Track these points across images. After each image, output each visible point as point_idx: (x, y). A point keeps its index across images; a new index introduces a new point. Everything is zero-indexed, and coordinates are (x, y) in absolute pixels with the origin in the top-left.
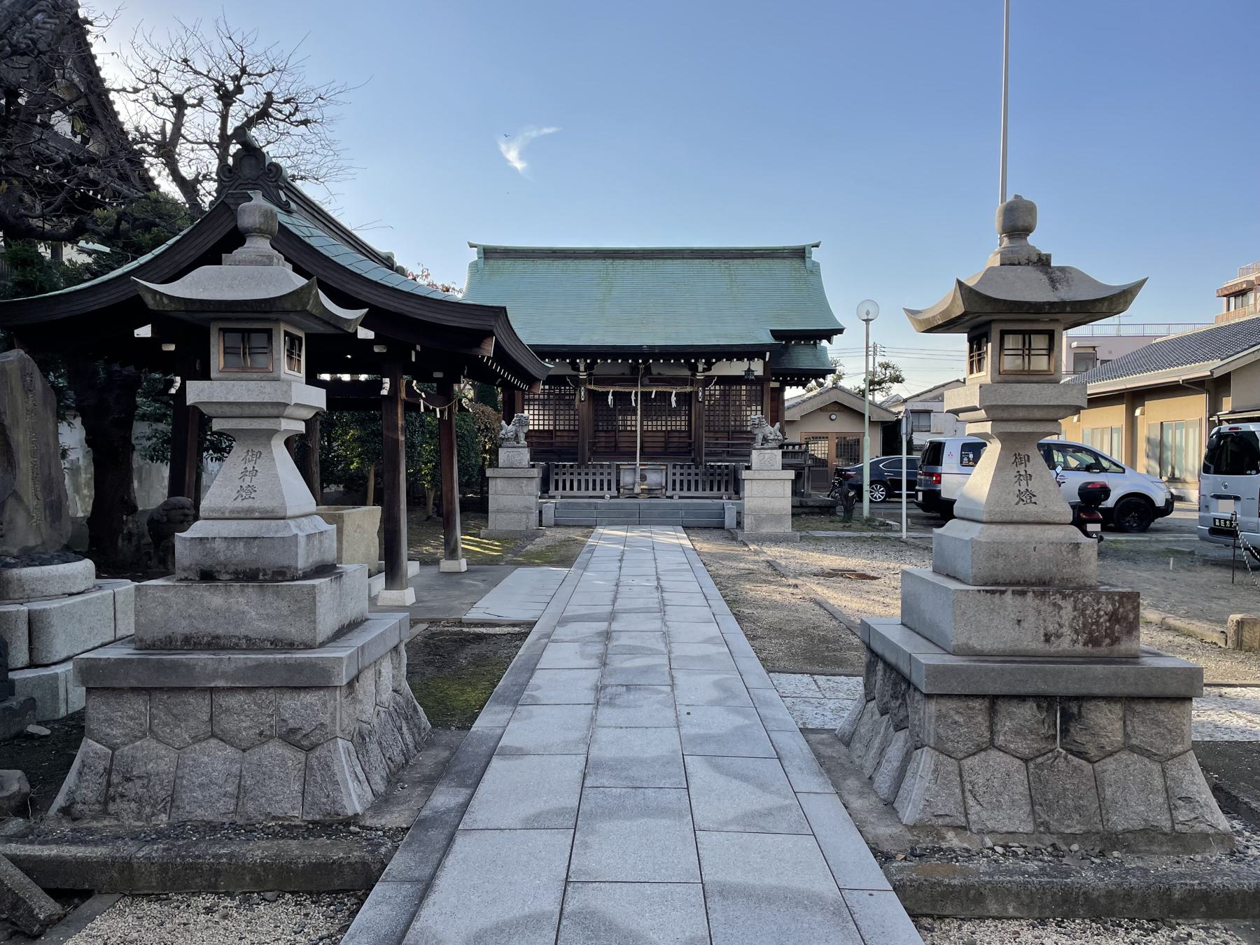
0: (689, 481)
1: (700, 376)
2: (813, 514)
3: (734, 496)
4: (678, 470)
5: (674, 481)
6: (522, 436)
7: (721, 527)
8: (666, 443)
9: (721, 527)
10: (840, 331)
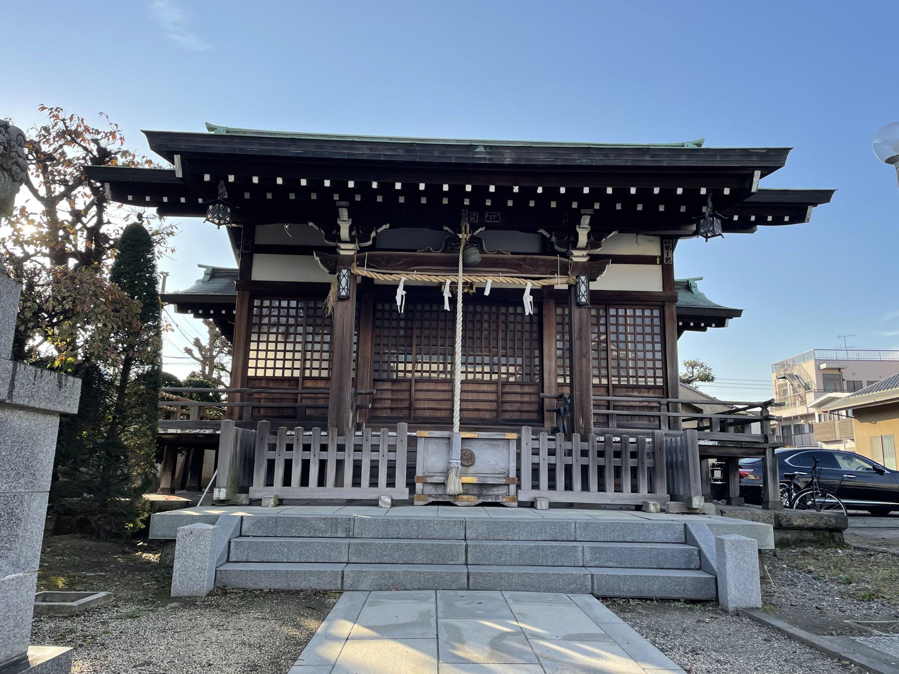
0: (568, 469)
2: (799, 543)
7: (708, 600)
8: (500, 403)
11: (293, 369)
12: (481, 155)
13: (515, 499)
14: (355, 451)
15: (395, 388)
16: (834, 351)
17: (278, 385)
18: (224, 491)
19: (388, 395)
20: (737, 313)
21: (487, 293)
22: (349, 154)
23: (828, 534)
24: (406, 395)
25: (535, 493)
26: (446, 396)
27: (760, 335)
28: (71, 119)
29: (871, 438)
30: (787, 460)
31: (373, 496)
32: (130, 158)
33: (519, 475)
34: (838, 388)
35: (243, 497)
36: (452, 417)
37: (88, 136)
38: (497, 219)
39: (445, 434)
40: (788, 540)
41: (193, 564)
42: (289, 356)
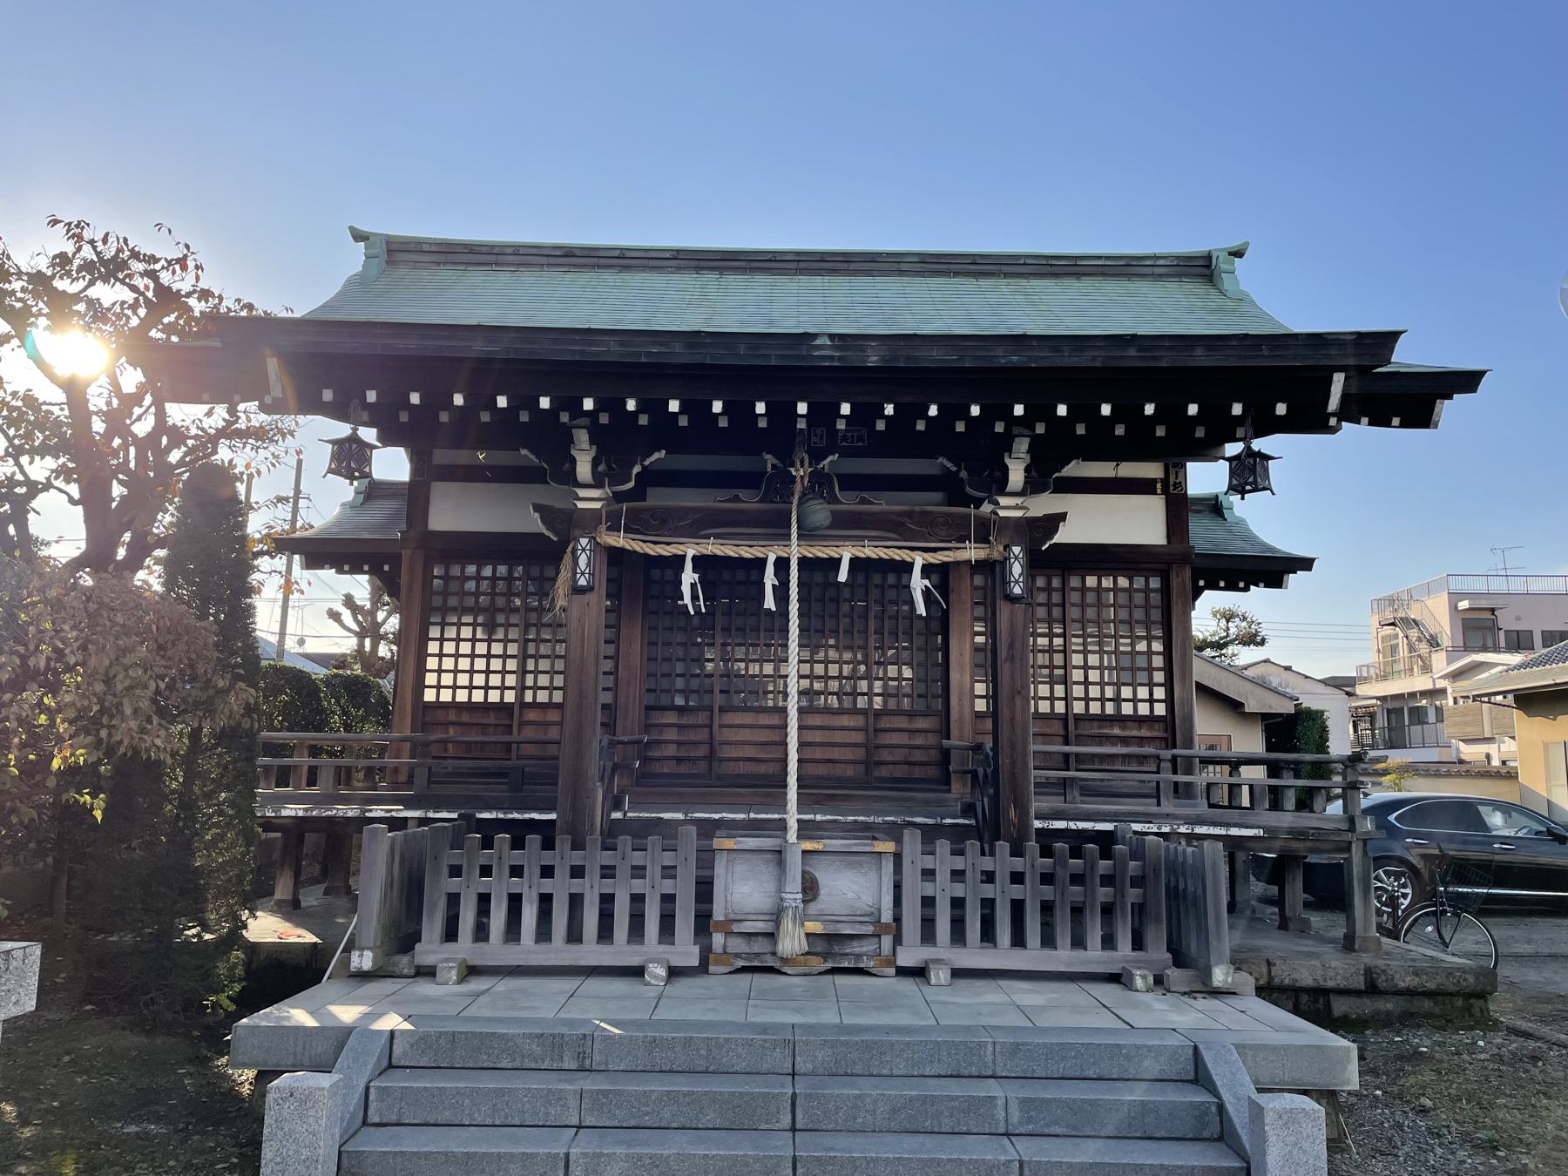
0: (1018, 908)
3: (1173, 974)
5: (928, 902)
8: (870, 747)
11: (503, 688)
12: (824, 351)
13: (891, 961)
14: (603, 877)
15: (684, 721)
16: (1485, 576)
17: (478, 718)
18: (368, 955)
19: (671, 735)
20: (1306, 564)
21: (843, 576)
22: (582, 352)
23: (1459, 1002)
24: (702, 735)
26: (775, 737)
27: (1343, 588)
28: (105, 241)
29: (1546, 746)
30: (1392, 818)
31: (634, 961)
32: (212, 302)
33: (897, 919)
34: (1490, 643)
35: (403, 962)
36: (786, 774)
37: (138, 266)
38: (860, 439)
40: (1388, 1013)
41: (296, 1152)
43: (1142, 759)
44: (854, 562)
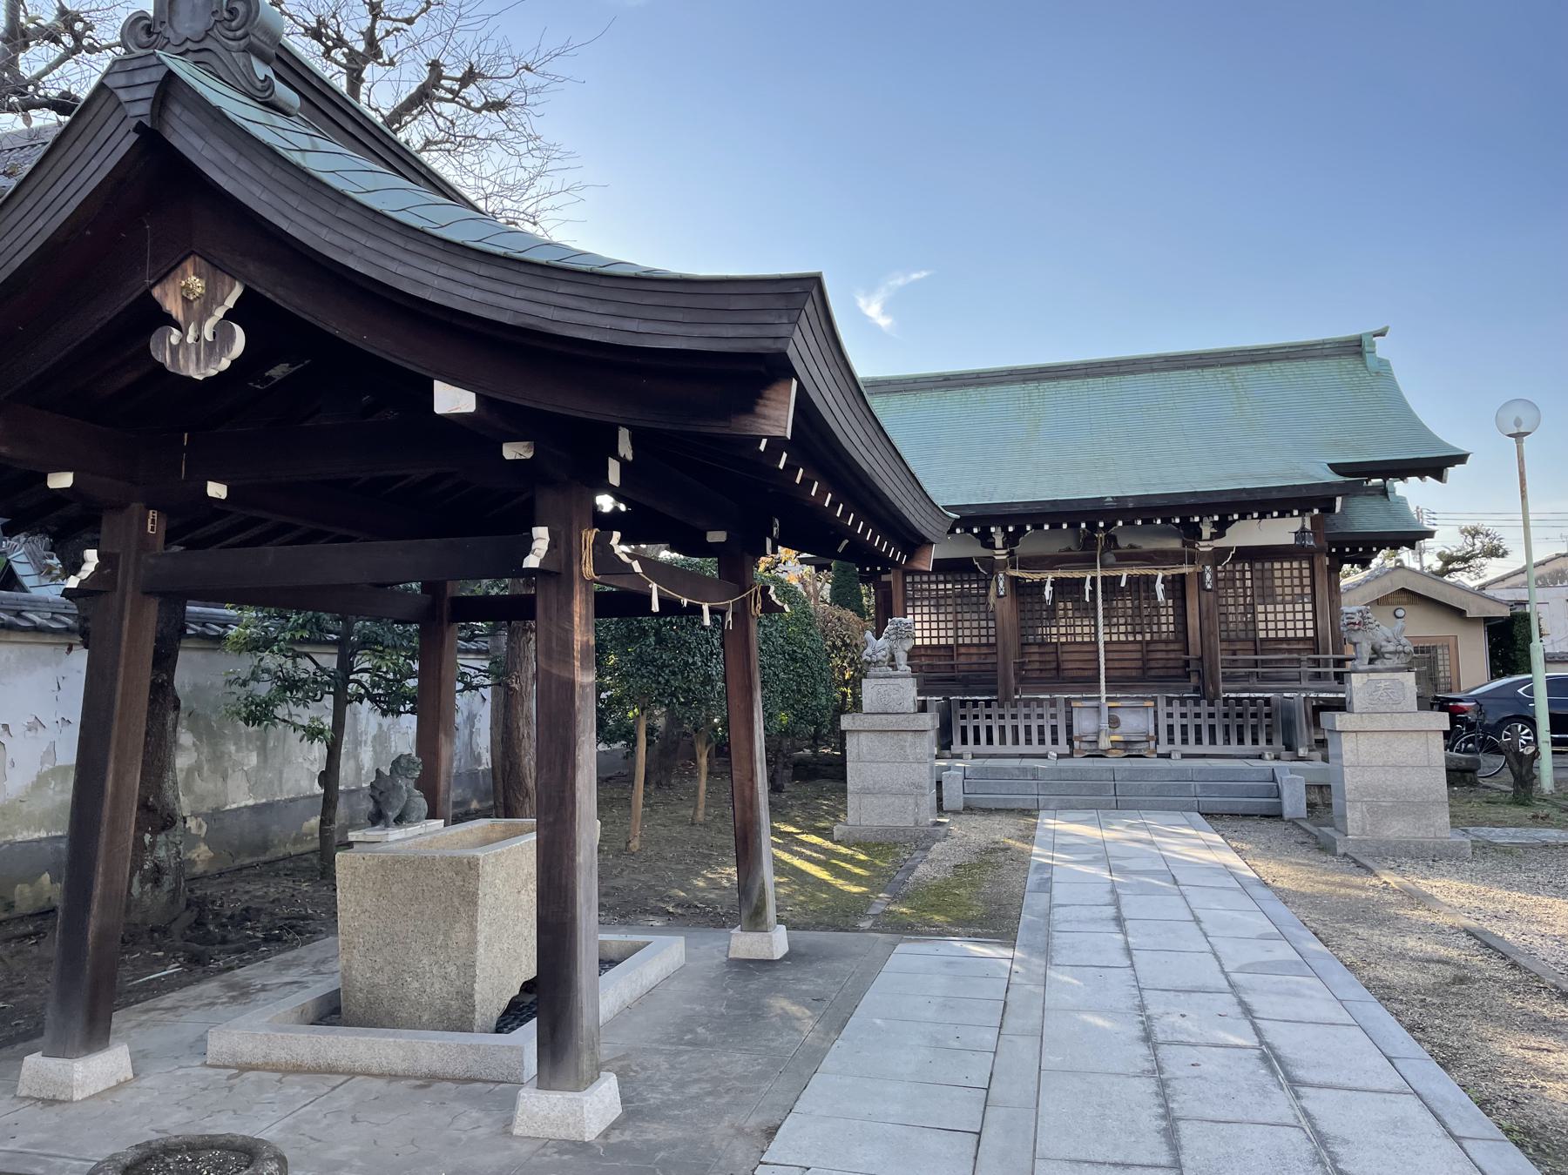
1: (1204, 547)
3: (1284, 754)
4: (1176, 709)
5: (1170, 728)
6: (902, 658)
7: (1275, 815)
9: (1275, 815)
10: (1461, 459)
11: (947, 637)
12: (1109, 504)
13: (1154, 751)
17: (936, 652)
21: (1123, 584)
25: (1171, 747)
33: (1156, 732)
35: (947, 752)
39: (1094, 703)
42: (942, 625)
43: (1291, 660)
44: (1130, 578)
